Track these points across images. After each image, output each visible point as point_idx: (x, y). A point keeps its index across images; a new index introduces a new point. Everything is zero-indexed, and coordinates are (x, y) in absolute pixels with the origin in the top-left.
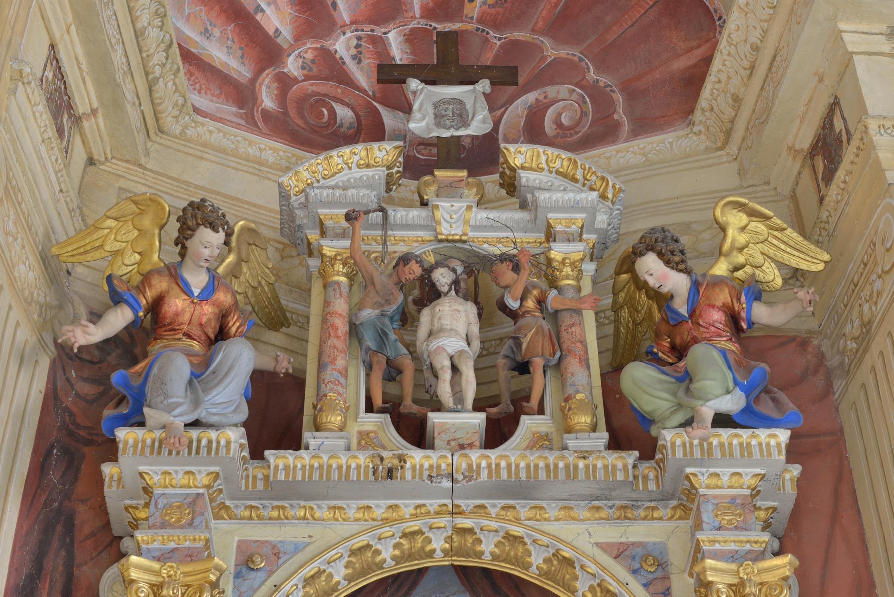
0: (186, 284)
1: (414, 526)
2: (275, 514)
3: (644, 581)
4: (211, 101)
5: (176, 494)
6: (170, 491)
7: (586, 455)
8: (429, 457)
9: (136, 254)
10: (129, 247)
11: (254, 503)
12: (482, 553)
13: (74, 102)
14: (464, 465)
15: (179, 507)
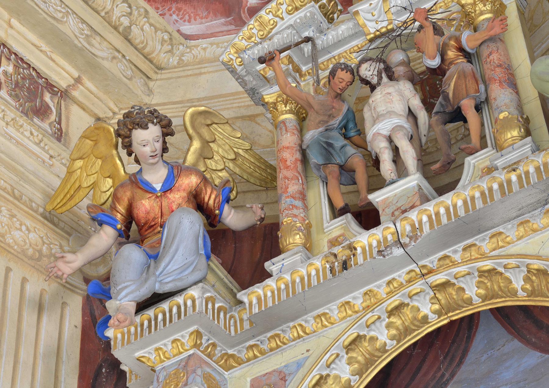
0: (147, 184)
1: (394, 302)
4: (201, 23)
5: (172, 364)
6: (167, 363)
7: (515, 166)
8: (374, 234)
9: (108, 179)
10: (100, 176)
11: (251, 342)
12: (471, 299)
13: (52, 81)
14: (408, 228)
15: (175, 374)
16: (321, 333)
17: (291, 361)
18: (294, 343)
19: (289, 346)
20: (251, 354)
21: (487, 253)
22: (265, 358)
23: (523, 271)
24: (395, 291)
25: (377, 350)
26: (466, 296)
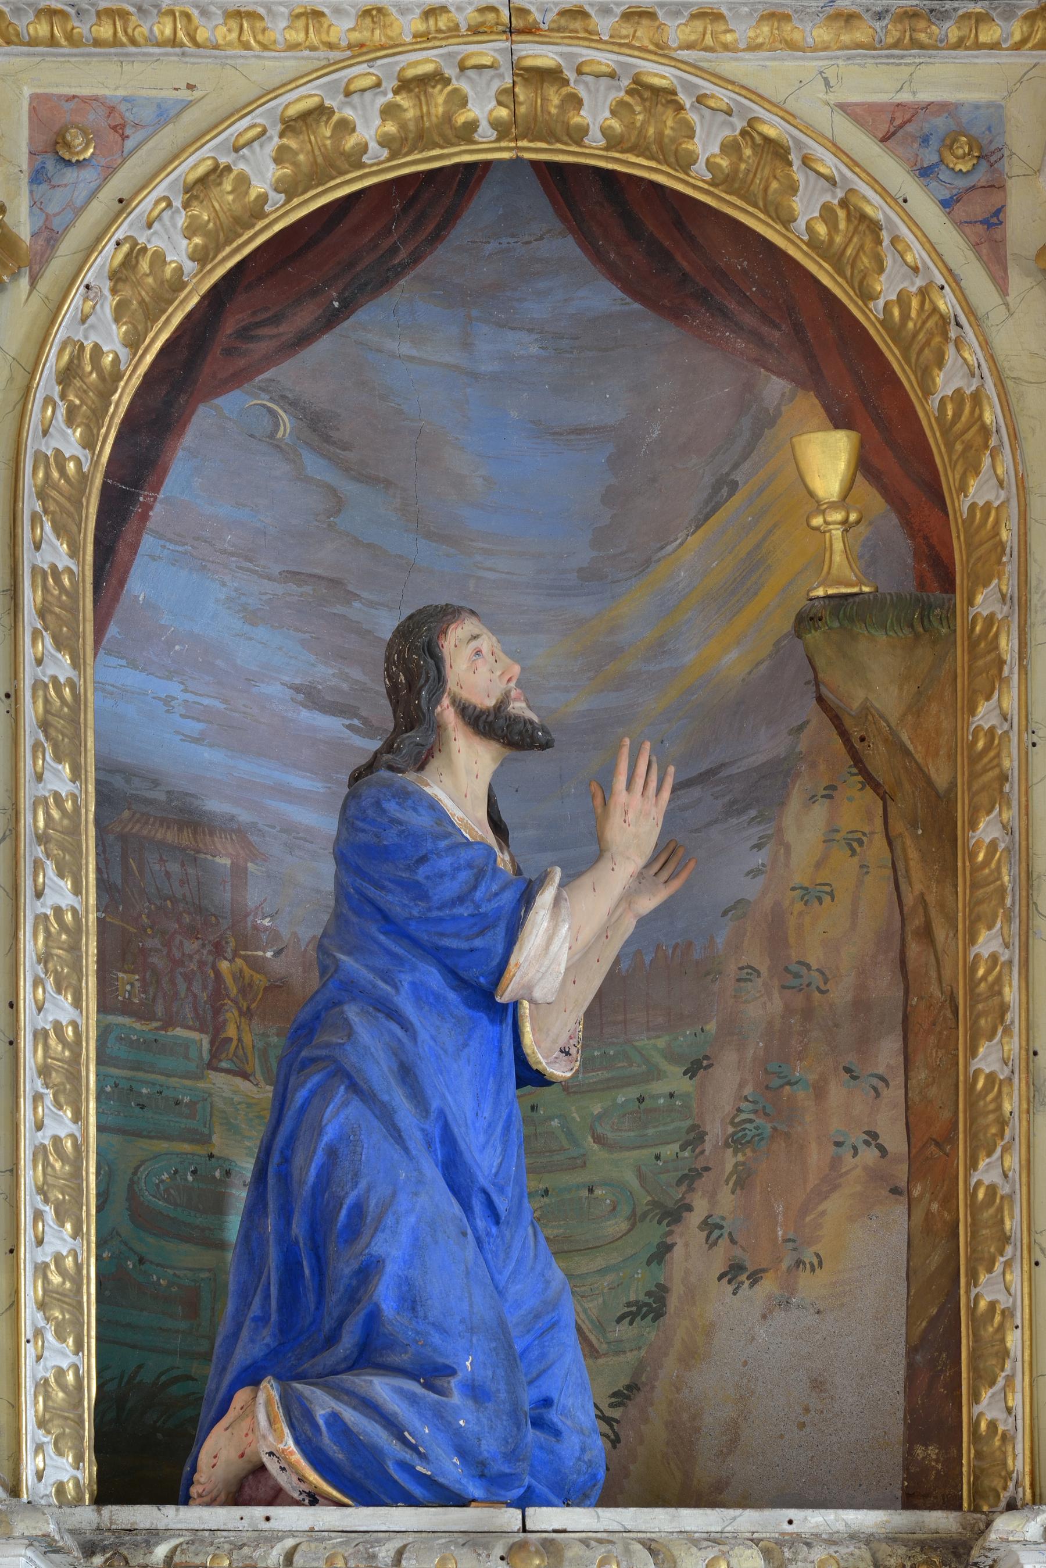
1: (422, 62)
2: (105, 31)
3: (946, 194)
12: (584, 131)
16: (231, 57)
17: (144, 93)
18: (157, 50)
19: (145, 54)
20: (42, 29)
21: (670, 48)
22: (75, 55)
23: (732, 126)
24: (435, 38)
25: (343, 153)
26: (576, 120)
